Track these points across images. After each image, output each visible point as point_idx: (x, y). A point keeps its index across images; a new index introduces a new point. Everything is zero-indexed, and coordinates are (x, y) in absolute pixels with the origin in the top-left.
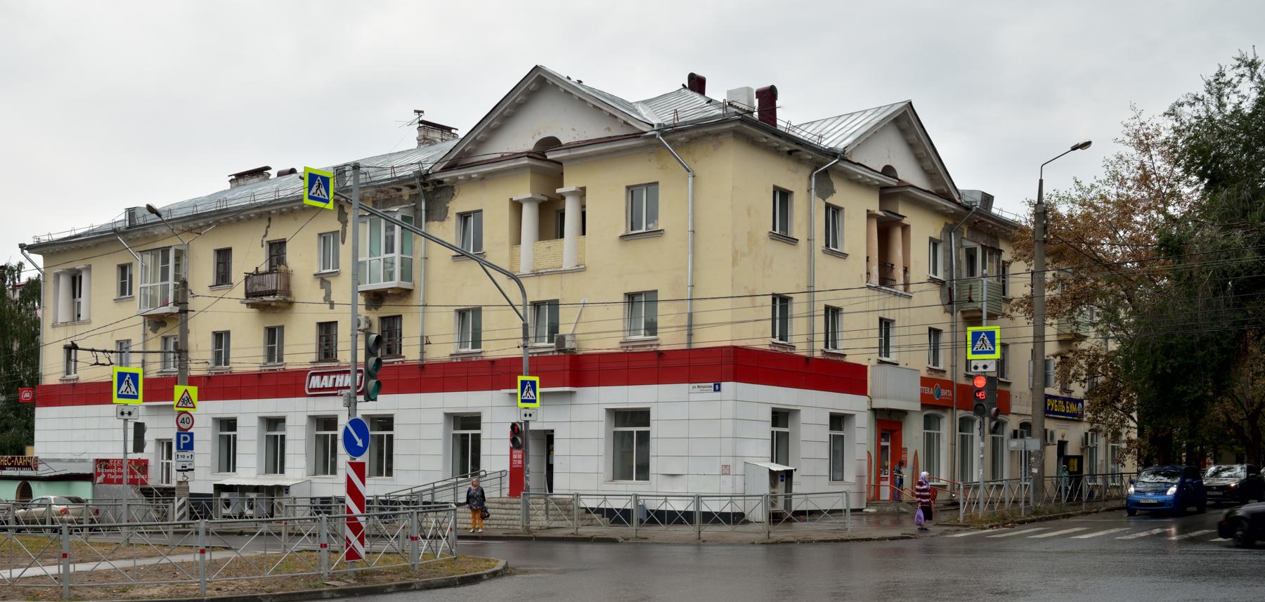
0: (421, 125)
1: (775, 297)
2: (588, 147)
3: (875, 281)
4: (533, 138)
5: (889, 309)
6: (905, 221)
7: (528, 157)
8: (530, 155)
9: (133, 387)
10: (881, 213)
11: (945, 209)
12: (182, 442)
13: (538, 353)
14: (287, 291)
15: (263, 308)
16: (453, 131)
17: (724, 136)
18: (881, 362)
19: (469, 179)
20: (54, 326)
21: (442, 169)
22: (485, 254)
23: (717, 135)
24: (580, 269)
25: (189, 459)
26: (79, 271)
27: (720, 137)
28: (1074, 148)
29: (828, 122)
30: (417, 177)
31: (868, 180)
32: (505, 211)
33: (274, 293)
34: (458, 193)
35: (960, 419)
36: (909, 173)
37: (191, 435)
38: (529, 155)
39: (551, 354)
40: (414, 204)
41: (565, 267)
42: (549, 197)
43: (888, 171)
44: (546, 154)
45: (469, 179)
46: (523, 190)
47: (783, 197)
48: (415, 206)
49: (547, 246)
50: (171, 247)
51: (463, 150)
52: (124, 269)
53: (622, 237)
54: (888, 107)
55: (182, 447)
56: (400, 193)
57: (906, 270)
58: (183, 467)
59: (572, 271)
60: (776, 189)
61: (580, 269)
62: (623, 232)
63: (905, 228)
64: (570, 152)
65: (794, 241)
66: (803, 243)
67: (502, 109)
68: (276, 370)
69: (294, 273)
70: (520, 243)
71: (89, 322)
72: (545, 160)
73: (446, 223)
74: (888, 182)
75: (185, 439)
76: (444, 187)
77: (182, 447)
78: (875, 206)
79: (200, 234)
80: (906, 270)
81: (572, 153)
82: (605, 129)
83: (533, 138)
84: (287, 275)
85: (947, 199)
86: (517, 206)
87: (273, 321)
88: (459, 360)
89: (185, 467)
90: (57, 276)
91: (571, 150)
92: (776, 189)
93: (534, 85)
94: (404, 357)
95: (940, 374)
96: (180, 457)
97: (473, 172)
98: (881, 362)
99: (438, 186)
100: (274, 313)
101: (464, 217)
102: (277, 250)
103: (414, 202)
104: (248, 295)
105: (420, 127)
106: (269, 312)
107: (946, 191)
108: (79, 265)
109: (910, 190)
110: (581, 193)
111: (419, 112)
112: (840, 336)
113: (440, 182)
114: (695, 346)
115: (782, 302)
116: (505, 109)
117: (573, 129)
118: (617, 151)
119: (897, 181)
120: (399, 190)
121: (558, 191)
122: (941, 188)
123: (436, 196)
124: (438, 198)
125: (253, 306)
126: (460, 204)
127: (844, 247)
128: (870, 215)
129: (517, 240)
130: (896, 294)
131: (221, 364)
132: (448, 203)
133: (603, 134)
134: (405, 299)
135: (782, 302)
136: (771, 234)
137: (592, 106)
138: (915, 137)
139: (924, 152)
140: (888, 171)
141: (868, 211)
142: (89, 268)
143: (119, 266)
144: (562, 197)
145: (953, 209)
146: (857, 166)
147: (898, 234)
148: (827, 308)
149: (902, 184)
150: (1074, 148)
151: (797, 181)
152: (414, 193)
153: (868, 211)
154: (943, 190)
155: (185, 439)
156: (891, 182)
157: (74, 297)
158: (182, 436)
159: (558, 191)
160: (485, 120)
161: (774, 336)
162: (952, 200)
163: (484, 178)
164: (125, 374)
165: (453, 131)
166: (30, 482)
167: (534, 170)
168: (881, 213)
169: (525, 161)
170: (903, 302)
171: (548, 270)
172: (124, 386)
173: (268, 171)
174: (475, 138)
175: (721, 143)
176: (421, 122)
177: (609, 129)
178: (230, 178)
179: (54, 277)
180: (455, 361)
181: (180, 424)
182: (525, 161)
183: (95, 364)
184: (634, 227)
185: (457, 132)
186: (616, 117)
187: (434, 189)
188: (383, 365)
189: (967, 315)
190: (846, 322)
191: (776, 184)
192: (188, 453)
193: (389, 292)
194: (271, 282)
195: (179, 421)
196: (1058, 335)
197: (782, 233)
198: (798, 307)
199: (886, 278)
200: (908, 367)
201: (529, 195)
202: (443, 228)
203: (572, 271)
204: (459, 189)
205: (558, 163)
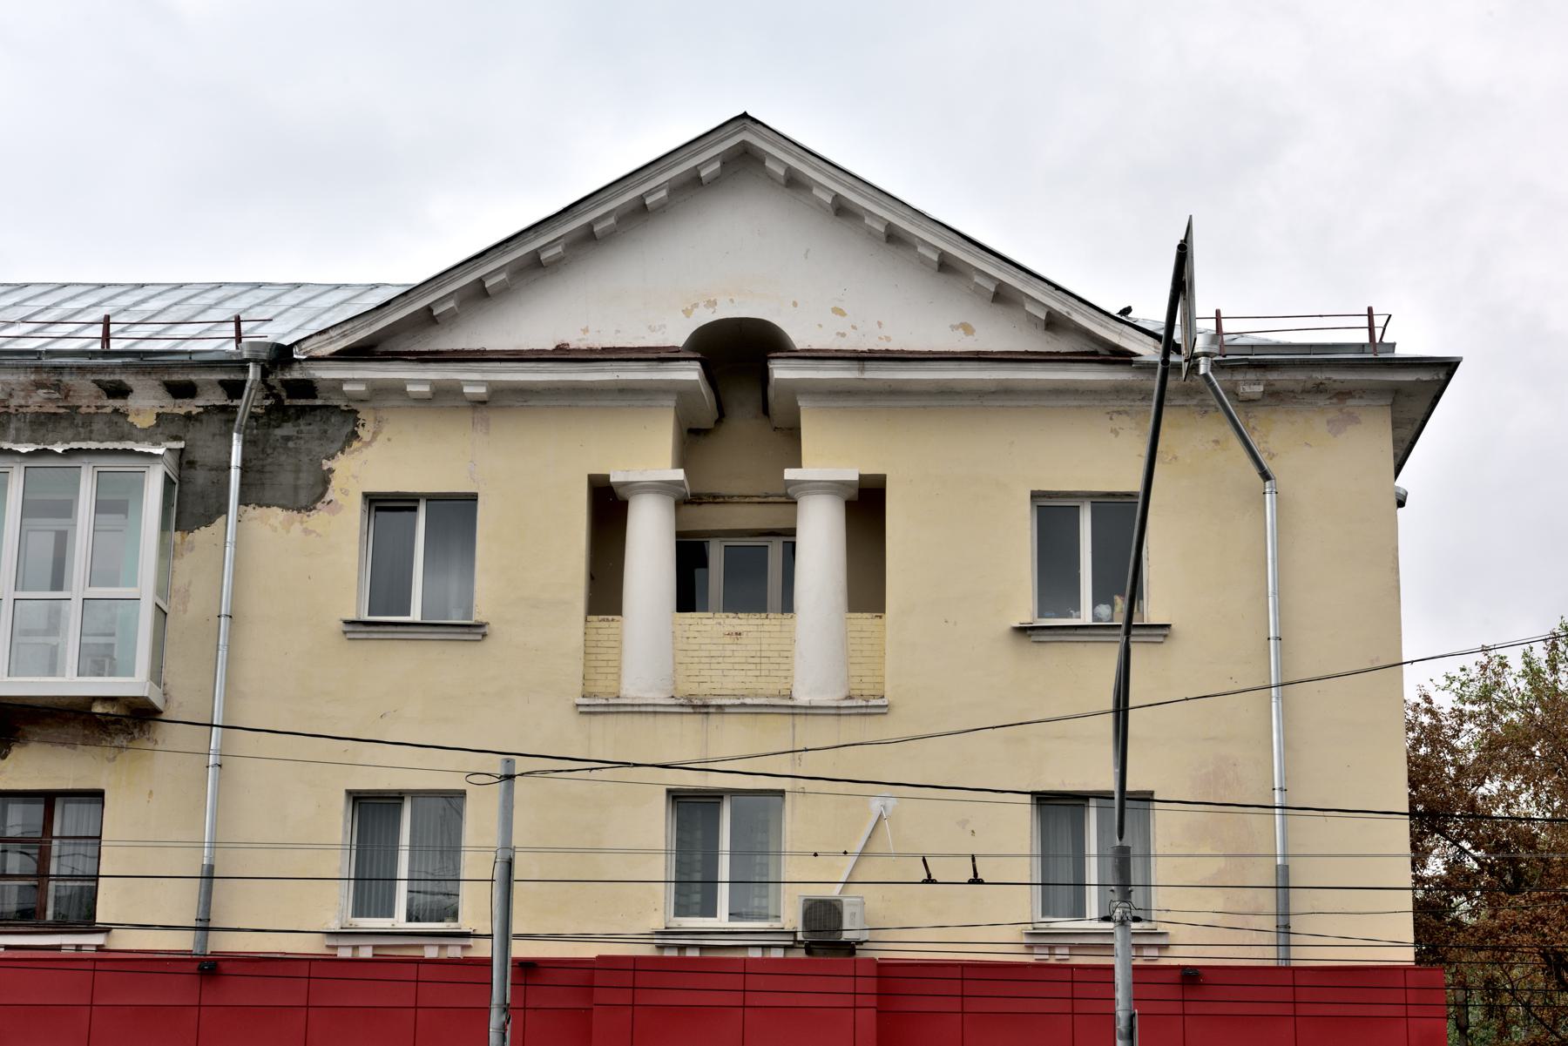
2: (1033, 366)
4: (687, 313)
5: (349, 879)
13: (702, 948)
17: (1363, 402)
21: (338, 353)
22: (486, 630)
23: (1343, 394)
27: (1351, 402)
29: (68, 292)
30: (256, 361)
34: (375, 435)
39: (756, 954)
40: (181, 445)
41: (802, 698)
48: (182, 450)
49: (728, 629)
53: (1023, 630)
54: (208, 287)
56: (118, 403)
64: (862, 370)
68: (58, 948)
73: (318, 519)
76: (314, 408)
81: (868, 375)
82: (953, 327)
88: (366, 953)
91: (868, 364)
99: (287, 402)
103: (177, 438)
113: (307, 388)
114: (1308, 955)
117: (839, 312)
118: (1006, 392)
120: (120, 391)
121: (790, 474)
123: (279, 432)
124: (287, 439)
132: (331, 457)
133: (1086, 349)
152: (182, 411)
159: (790, 474)
160: (531, 234)
171: (748, 701)
175: (1355, 420)
177: (967, 329)
180: (344, 953)
183: (924, 882)
187: (269, 409)
188: (803, 946)
191: (367, 490)
193: (98, 709)
202: (307, 532)
204: (378, 421)
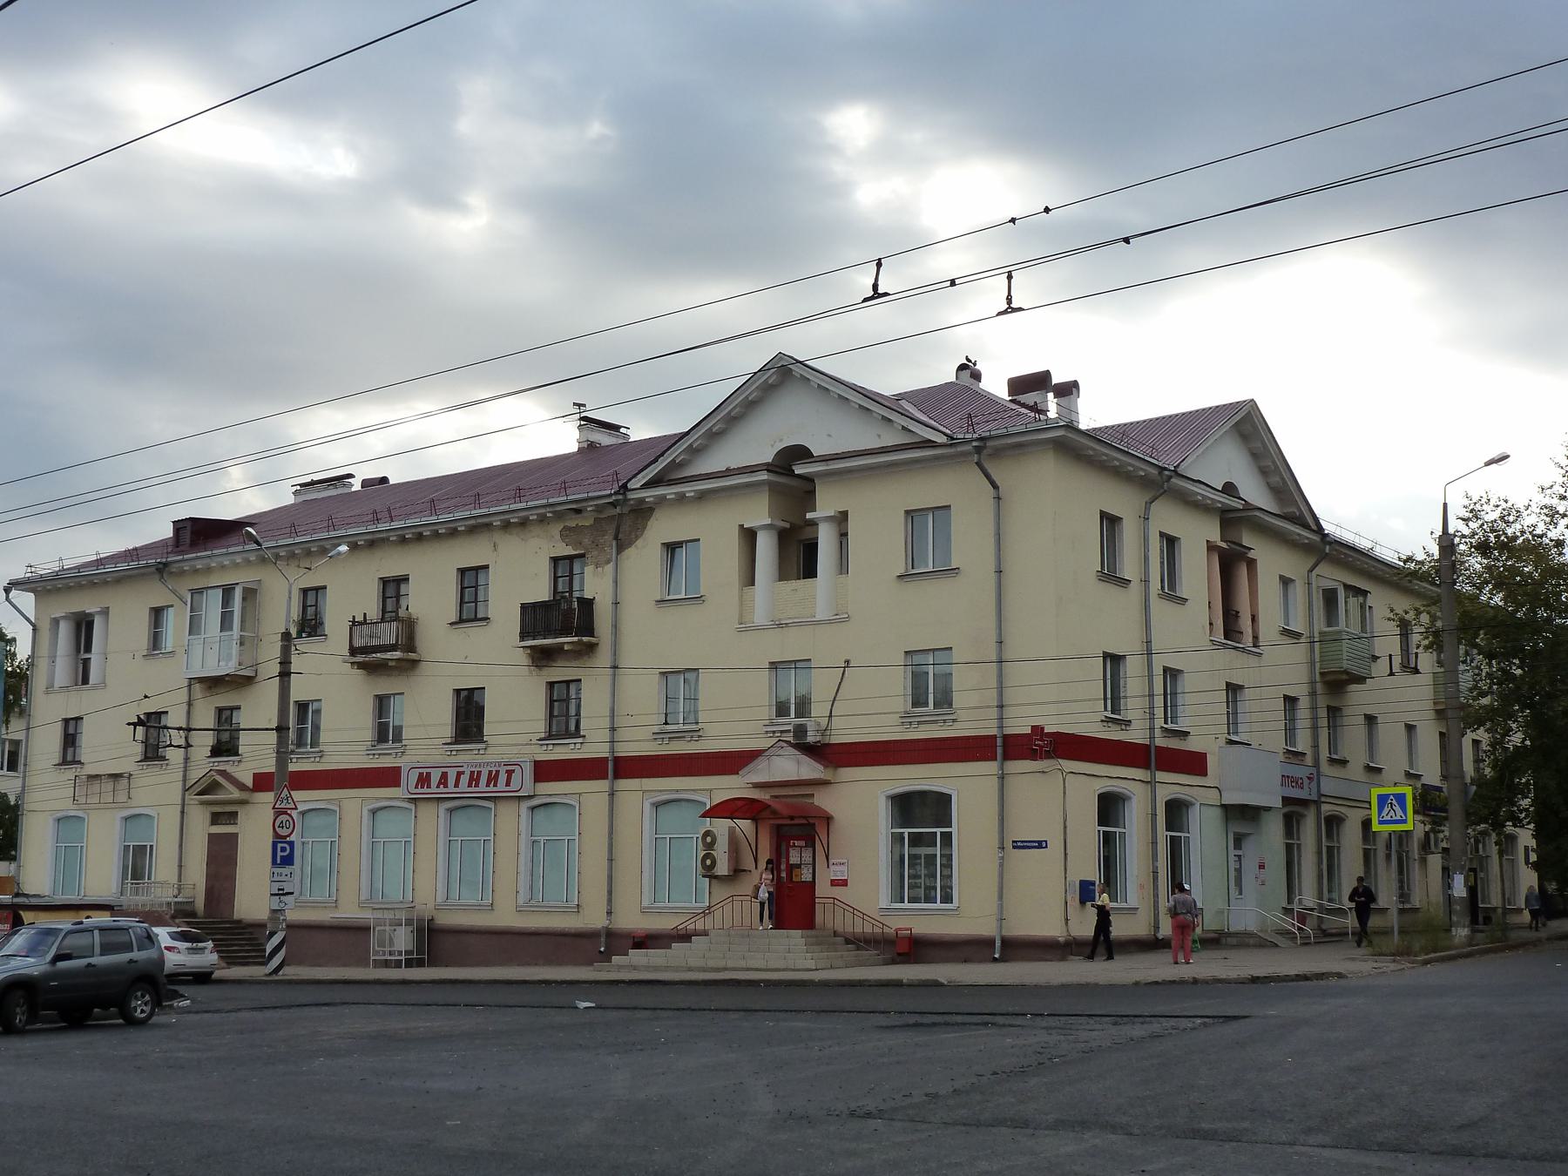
0: (582, 423)
1: (1107, 656)
3: (1220, 637)
6: (1251, 555)
7: (768, 471)
8: (770, 468)
9: (1397, 808)
10: (1224, 545)
11: (1298, 537)
12: (279, 854)
14: (409, 642)
15: (373, 669)
16: (622, 430)
18: (1231, 742)
19: (681, 498)
20: (49, 688)
24: (840, 619)
25: (288, 878)
26: (91, 615)
28: (1488, 464)
31: (1209, 502)
32: (732, 545)
33: (393, 648)
35: (1325, 818)
36: (1253, 492)
37: (291, 844)
38: (769, 468)
42: (791, 524)
43: (1229, 489)
44: (794, 468)
45: (681, 498)
46: (758, 513)
47: (1110, 522)
50: (237, 584)
51: (674, 460)
52: (157, 613)
55: (279, 862)
57: (1254, 619)
58: (279, 890)
59: (830, 622)
60: (1103, 515)
61: (840, 619)
62: (902, 571)
63: (1251, 564)
65: (1125, 583)
66: (1135, 587)
67: (731, 407)
69: (420, 622)
70: (753, 584)
71: (103, 684)
72: (791, 473)
74: (1229, 502)
75: (283, 849)
77: (279, 862)
78: (1214, 534)
79: (310, 569)
80: (1254, 619)
83: (772, 446)
84: (409, 626)
85: (1300, 525)
86: (749, 536)
87: (384, 686)
89: (283, 890)
90: (56, 622)
92: (1103, 515)
93: (775, 377)
94: (584, 736)
95: (1300, 758)
96: (276, 874)
97: (689, 489)
98: (1231, 742)
100: (389, 675)
101: (671, 548)
102: (392, 587)
104: (353, 651)
105: (580, 425)
106: (381, 675)
107: (1298, 514)
108: (91, 609)
109: (1257, 513)
110: (842, 518)
111: (580, 405)
112: (1299, 715)
115: (1114, 660)
116: (735, 407)
119: (1243, 502)
121: (809, 516)
122: (1291, 510)
125: (361, 666)
126: (662, 528)
127: (1183, 592)
128: (1211, 547)
129: (750, 579)
130: (1243, 650)
131: (306, 745)
134: (586, 658)
135: (1114, 660)
136: (1100, 574)
137: (857, 406)
138: (1260, 445)
139: (1270, 464)
140: (1229, 489)
141: (1160, 532)
142: (105, 612)
143: (152, 609)
144: (813, 524)
145: (1308, 538)
146: (1197, 484)
147: (1243, 571)
148: (1166, 670)
149: (1249, 507)
150: (1488, 464)
151: (1123, 502)
153: (1160, 532)
154: (1294, 512)
155: (283, 849)
156: (1236, 504)
157: (78, 651)
158: (279, 845)
159: (809, 516)
161: (1106, 709)
162: (1306, 526)
163: (702, 496)
164: (1388, 796)
165: (622, 430)
166: (21, 913)
167: (773, 488)
168: (1224, 545)
169: (764, 476)
170: (1253, 661)
172: (1386, 810)
173: (349, 480)
174: (691, 445)
176: (582, 419)
178: (295, 488)
179: (50, 624)
181: (277, 829)
182: (764, 476)
184: (915, 566)
185: (628, 432)
186: (890, 420)
189: (1328, 678)
190: (1187, 683)
192: (286, 870)
194: (388, 634)
195: (277, 824)
196: (1435, 703)
197: (1110, 575)
198: (1133, 669)
199: (1231, 631)
200: (1261, 748)
201: (768, 521)
203: (830, 622)
205: (809, 480)
